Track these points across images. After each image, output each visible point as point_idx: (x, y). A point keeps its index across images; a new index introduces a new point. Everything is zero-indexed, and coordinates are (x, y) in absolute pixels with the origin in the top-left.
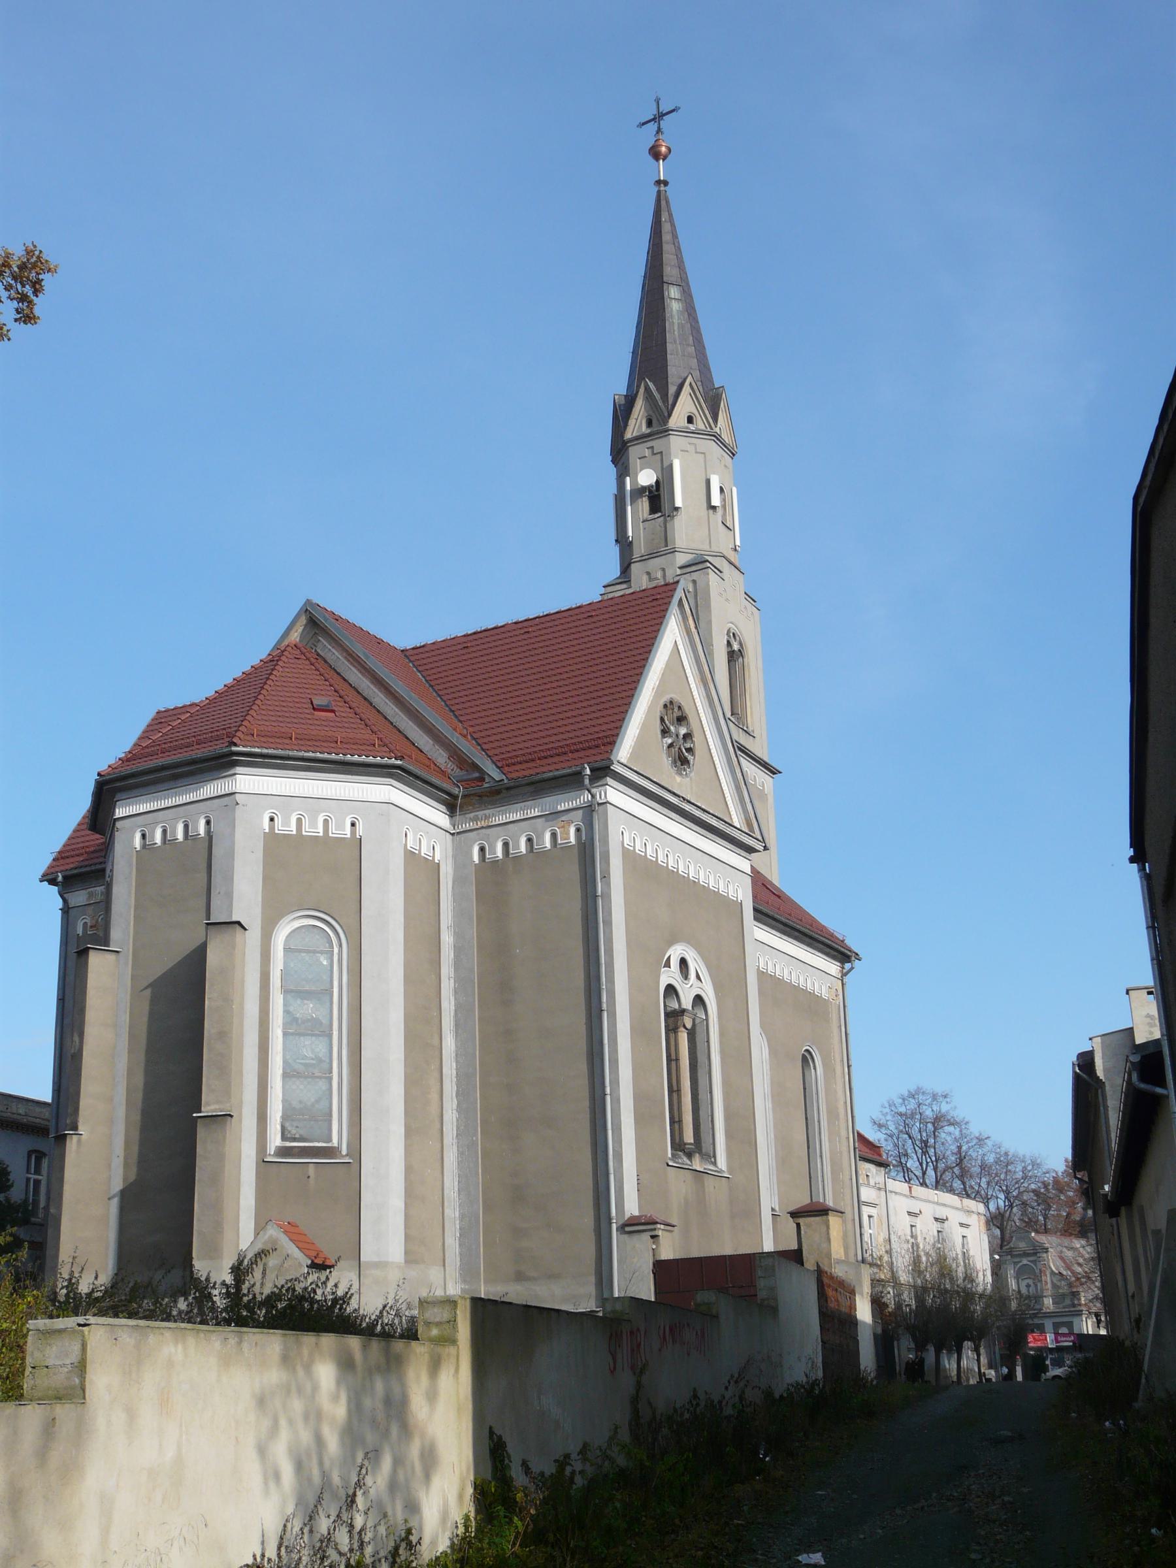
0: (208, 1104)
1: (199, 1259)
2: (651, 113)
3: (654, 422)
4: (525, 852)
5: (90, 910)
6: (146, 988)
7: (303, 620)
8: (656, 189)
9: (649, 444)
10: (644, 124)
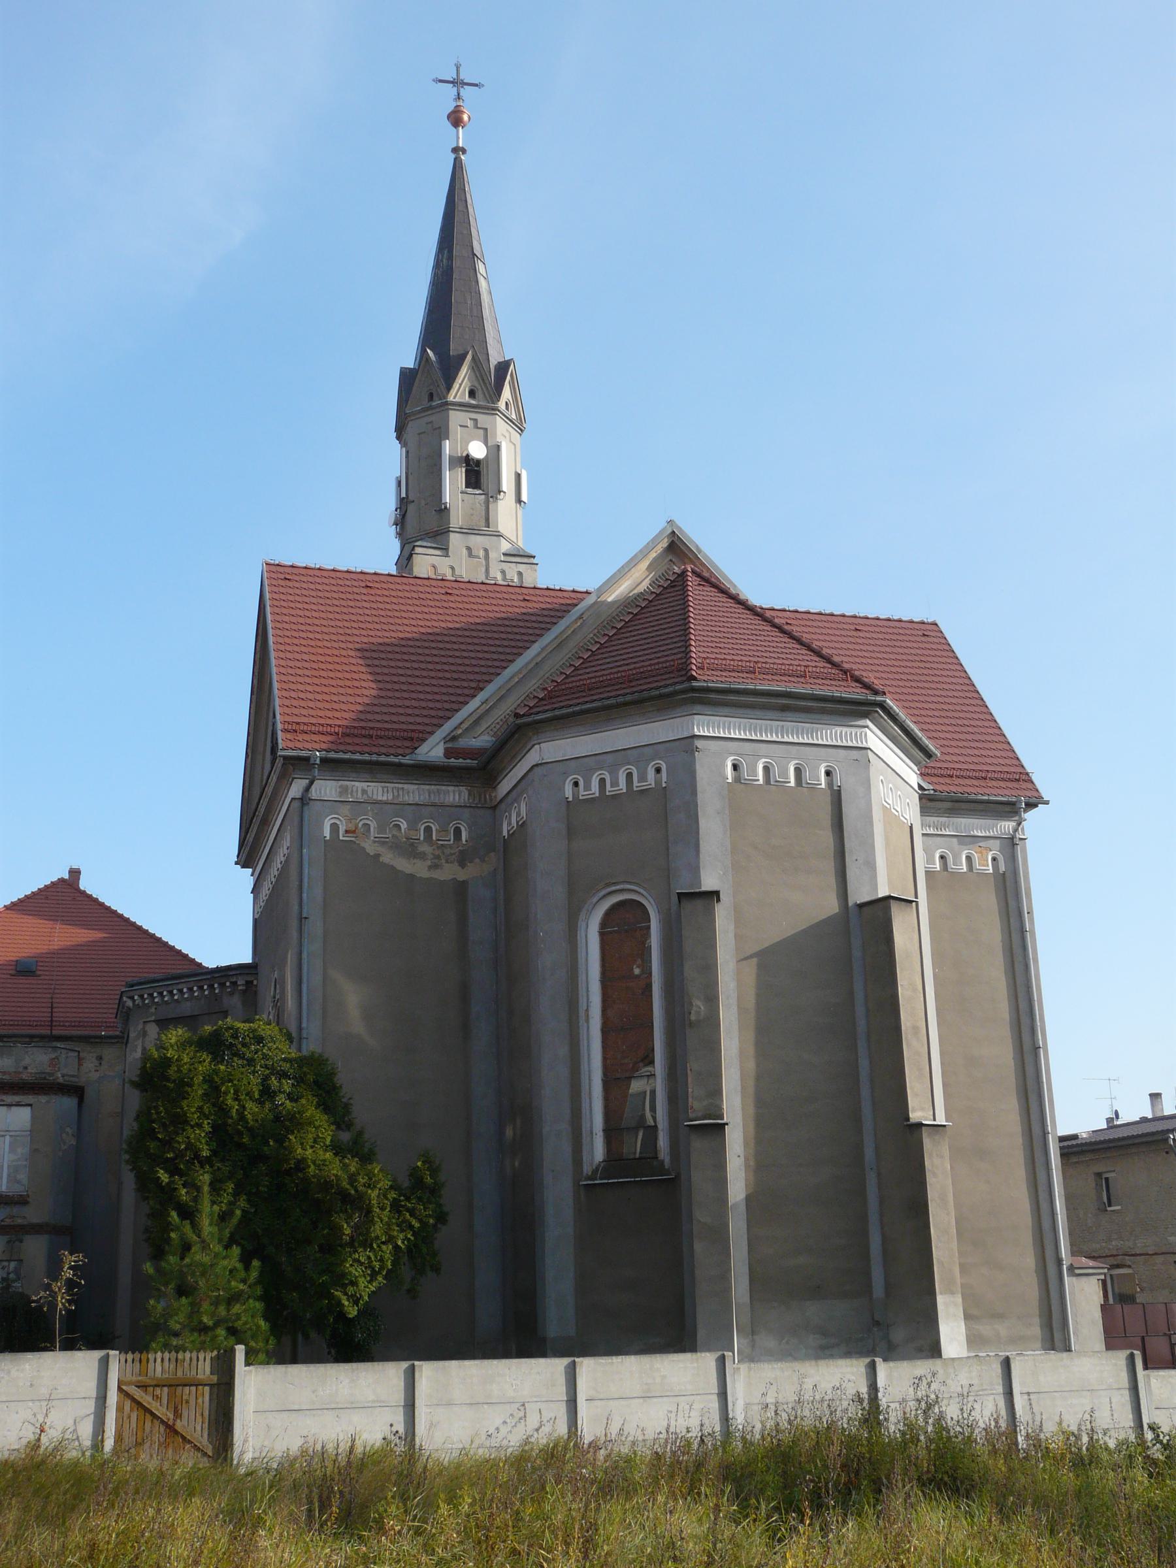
0: (914, 1111)
1: (941, 1294)
2: (450, 75)
3: (479, 394)
4: (938, 869)
5: (345, 809)
6: (751, 957)
7: (665, 544)
8: (453, 156)
9: (474, 416)
10: (476, 85)
